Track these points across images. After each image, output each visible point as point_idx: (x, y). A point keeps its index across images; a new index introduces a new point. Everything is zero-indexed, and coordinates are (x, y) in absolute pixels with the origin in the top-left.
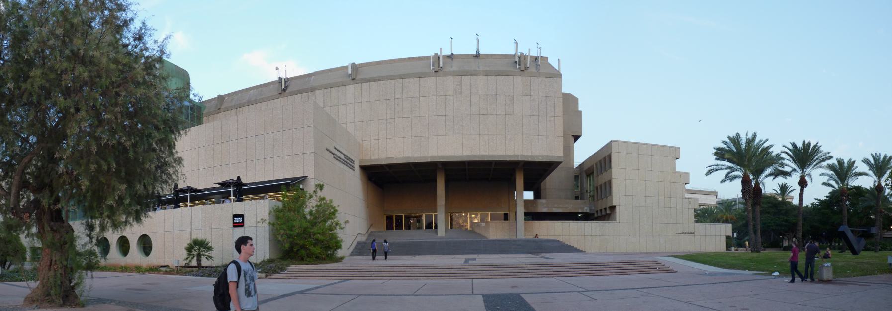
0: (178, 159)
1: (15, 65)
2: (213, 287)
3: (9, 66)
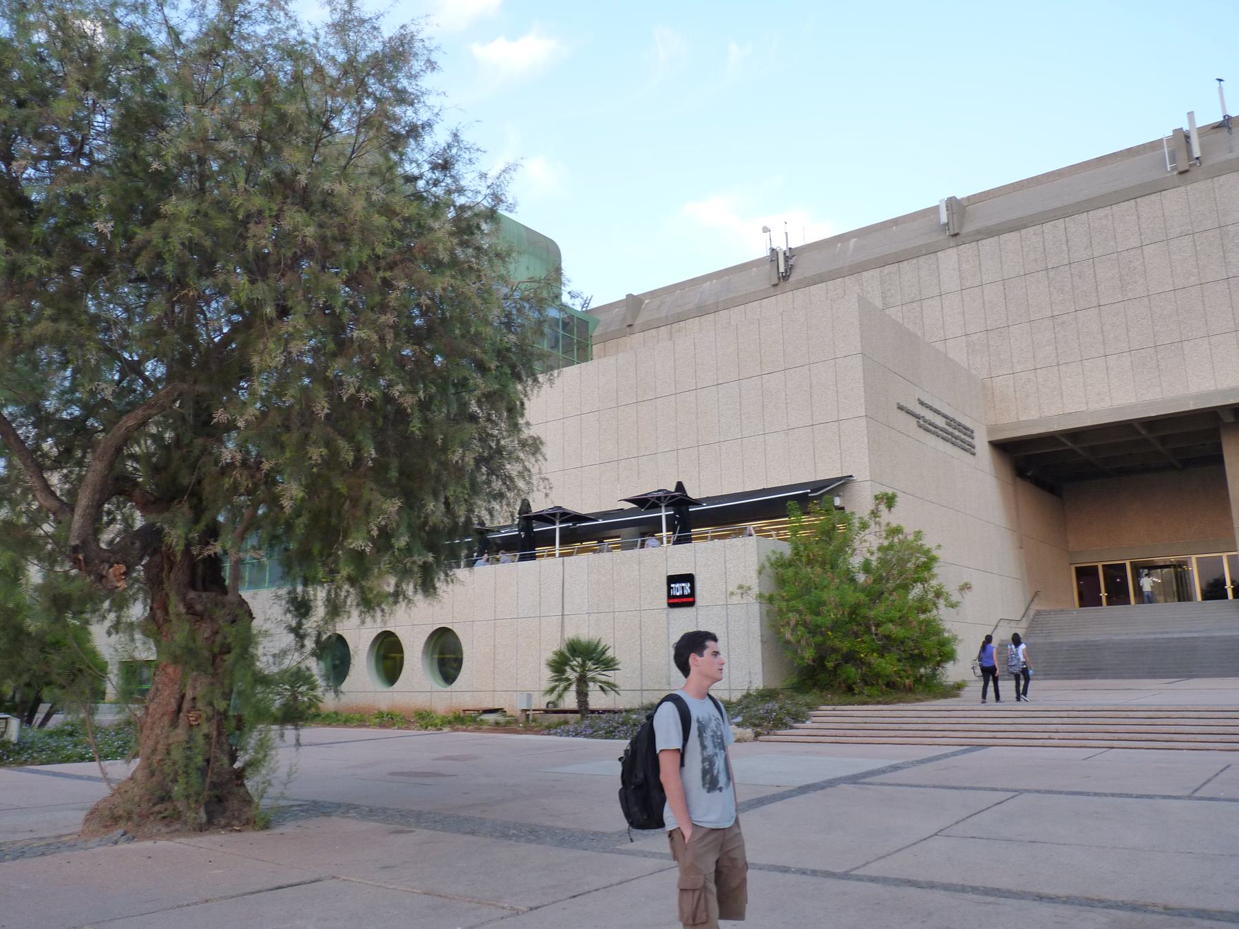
0: (530, 442)
1: (123, 178)
2: (620, 764)
3: (104, 177)
